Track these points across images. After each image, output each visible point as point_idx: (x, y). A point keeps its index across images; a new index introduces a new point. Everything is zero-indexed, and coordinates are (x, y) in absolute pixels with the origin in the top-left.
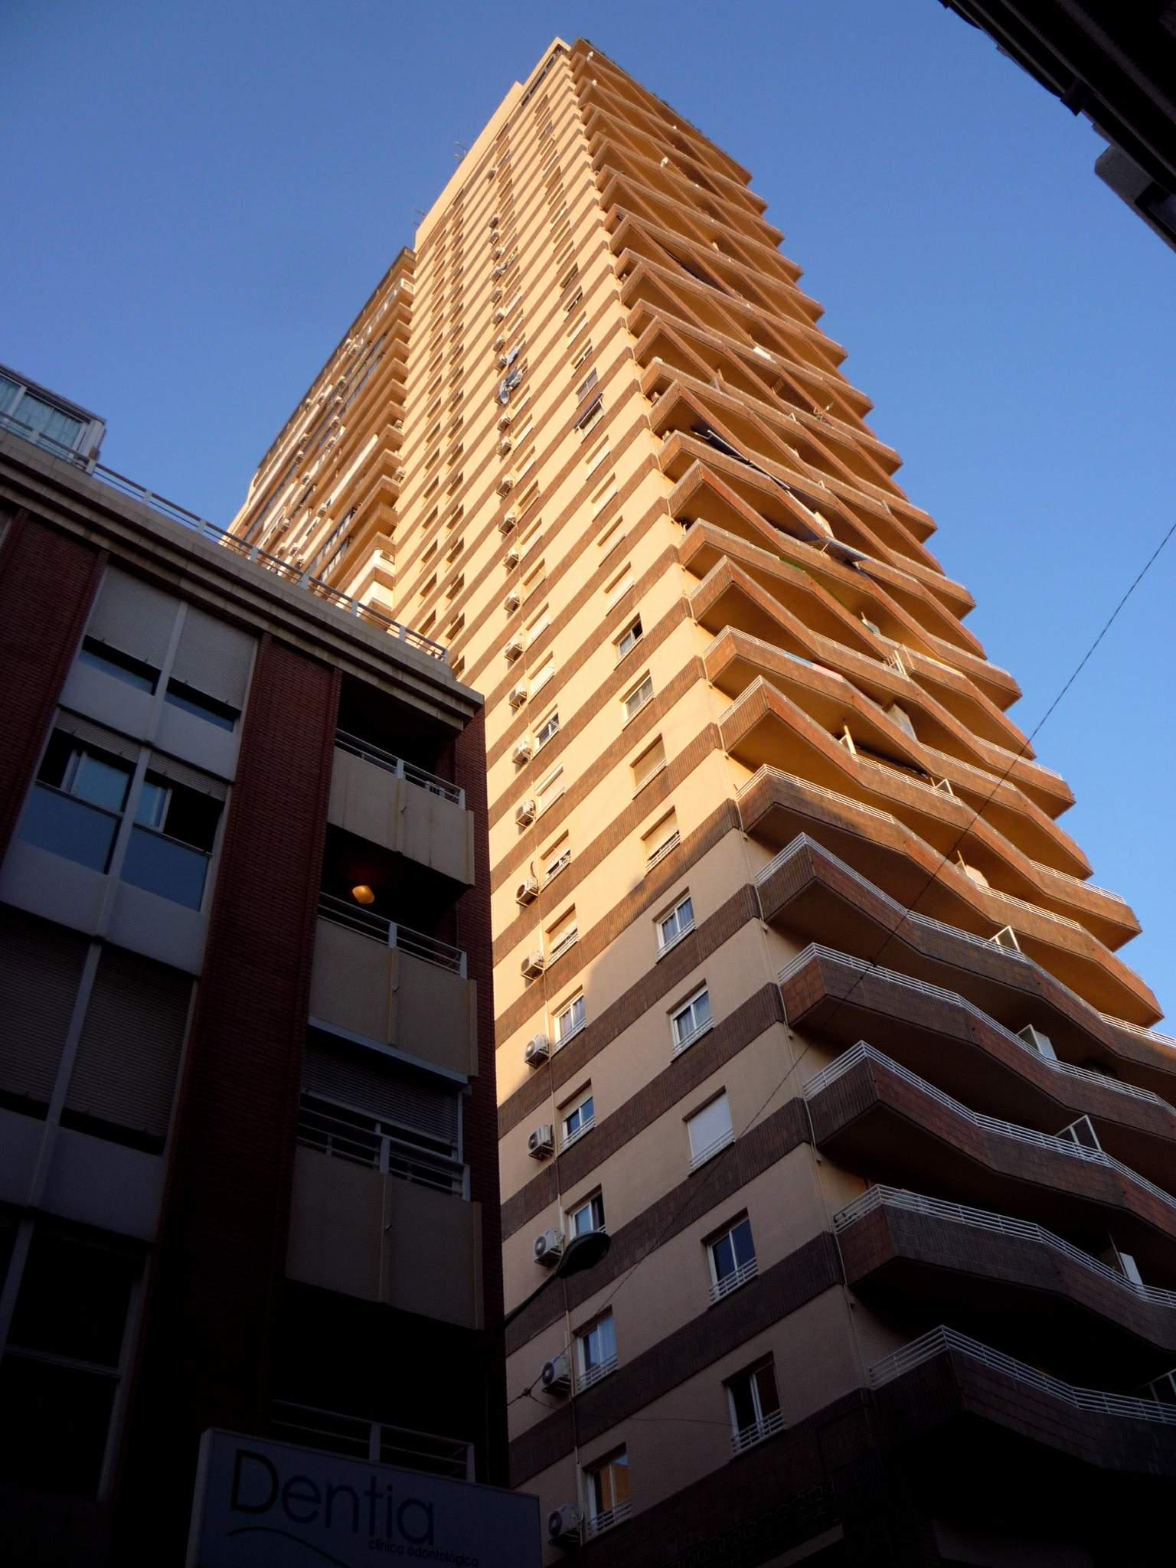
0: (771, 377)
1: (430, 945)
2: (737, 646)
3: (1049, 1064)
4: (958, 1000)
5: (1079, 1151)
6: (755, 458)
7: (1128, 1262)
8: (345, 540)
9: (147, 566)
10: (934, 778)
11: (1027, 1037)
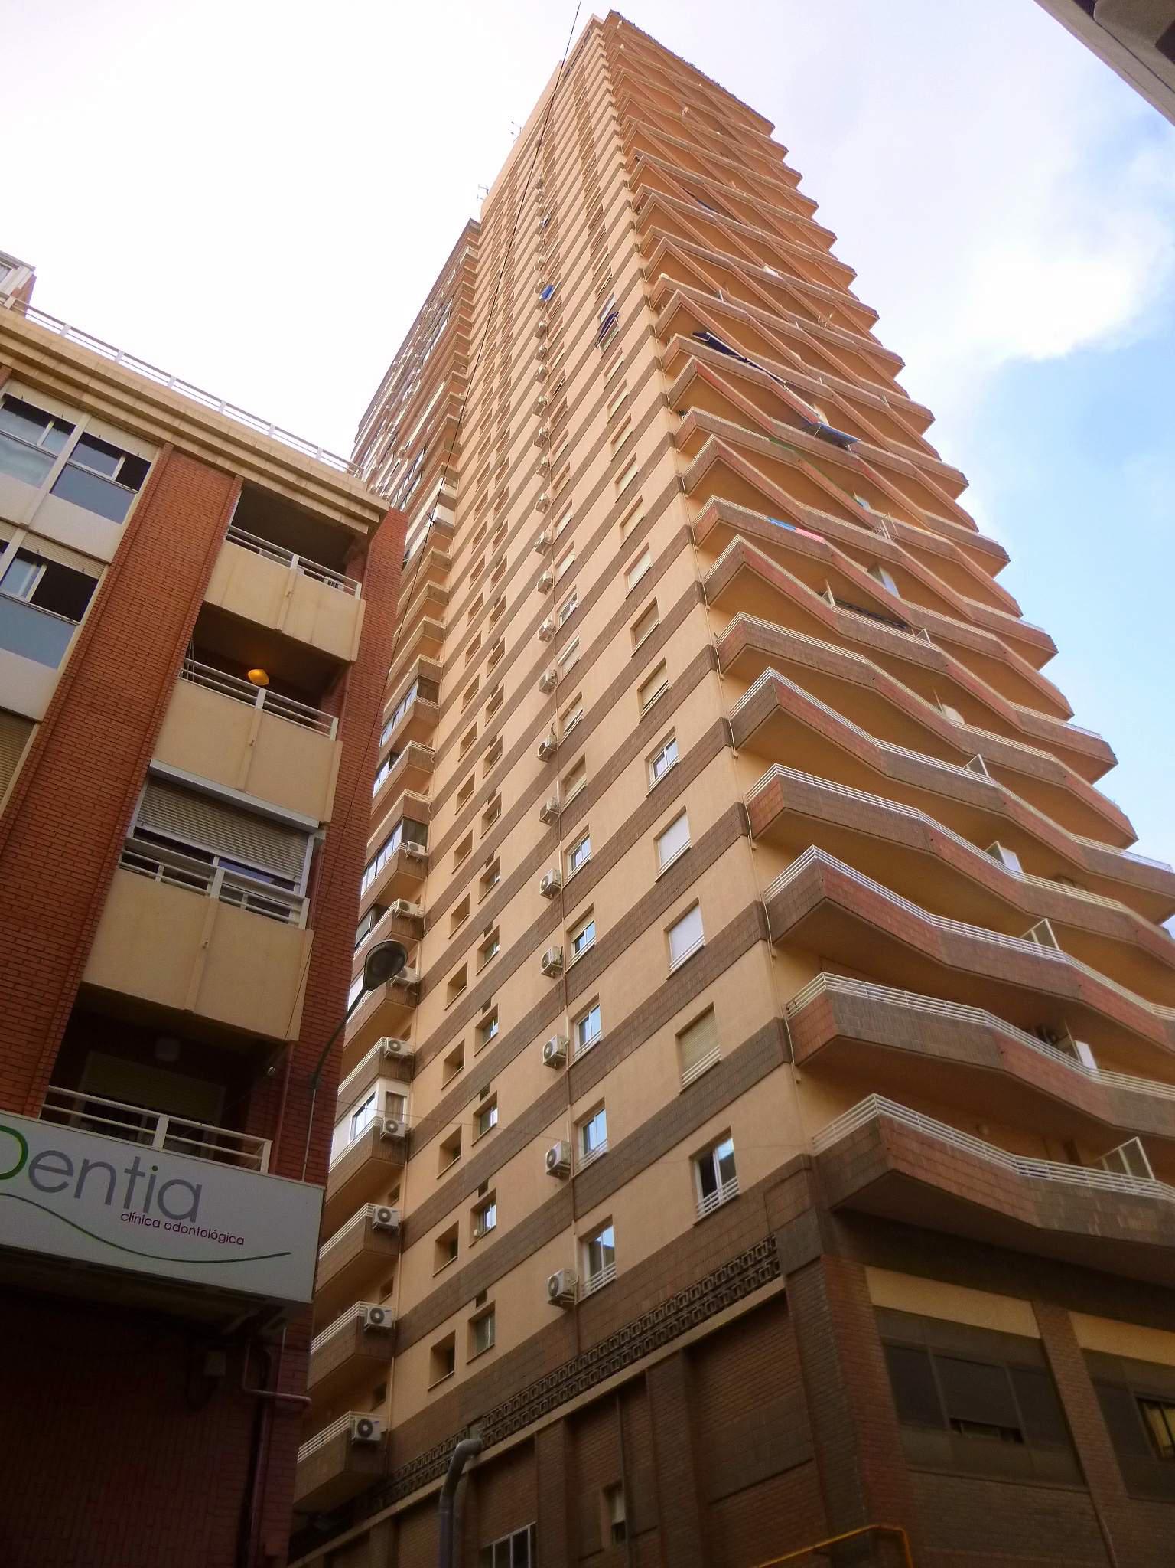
0: (776, 289)
1: (314, 717)
2: (720, 513)
3: (1014, 876)
4: (919, 815)
5: (1036, 949)
6: (753, 358)
7: (1084, 1049)
8: (418, 474)
9: (49, 381)
10: (914, 629)
11: (997, 856)
